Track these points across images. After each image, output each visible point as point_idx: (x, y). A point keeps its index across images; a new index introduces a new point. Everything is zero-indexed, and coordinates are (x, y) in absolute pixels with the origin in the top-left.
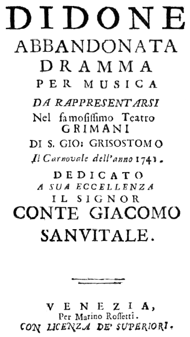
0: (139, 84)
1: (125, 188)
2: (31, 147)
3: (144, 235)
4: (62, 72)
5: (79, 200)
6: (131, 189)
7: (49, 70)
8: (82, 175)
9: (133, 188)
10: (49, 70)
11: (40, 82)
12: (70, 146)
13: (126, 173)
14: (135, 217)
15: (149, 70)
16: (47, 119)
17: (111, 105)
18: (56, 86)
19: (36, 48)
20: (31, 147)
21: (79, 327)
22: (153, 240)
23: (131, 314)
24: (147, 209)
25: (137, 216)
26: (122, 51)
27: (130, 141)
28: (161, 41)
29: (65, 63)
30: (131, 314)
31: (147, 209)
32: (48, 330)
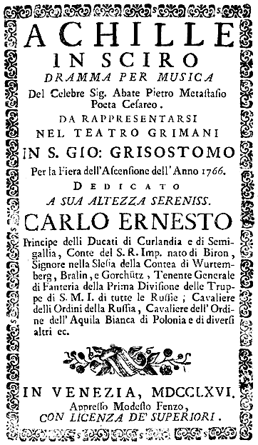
0: (134, 187)
1: (133, 79)
2: (75, 189)
3: (71, 392)
4: (147, 52)
5: (52, 150)
6: (87, 388)
7: (68, 23)
8: (78, 186)
9: (83, 394)
10: (68, 23)
11: (104, 117)
12: (82, 156)
13: (183, 148)
14: (89, 228)
15: (198, 136)
16: (41, 95)
17: (70, 395)
18: (73, 396)
19: (207, 254)
20: (75, 189)
21: (133, 203)
22: (233, 397)
23: (115, 239)
24: (95, 226)
25: (92, 227)
26: (117, 45)
27: (183, 148)
28: (188, 148)
29: (165, 57)
30: (115, 239)
31: (95, 226)
32: (46, 81)
